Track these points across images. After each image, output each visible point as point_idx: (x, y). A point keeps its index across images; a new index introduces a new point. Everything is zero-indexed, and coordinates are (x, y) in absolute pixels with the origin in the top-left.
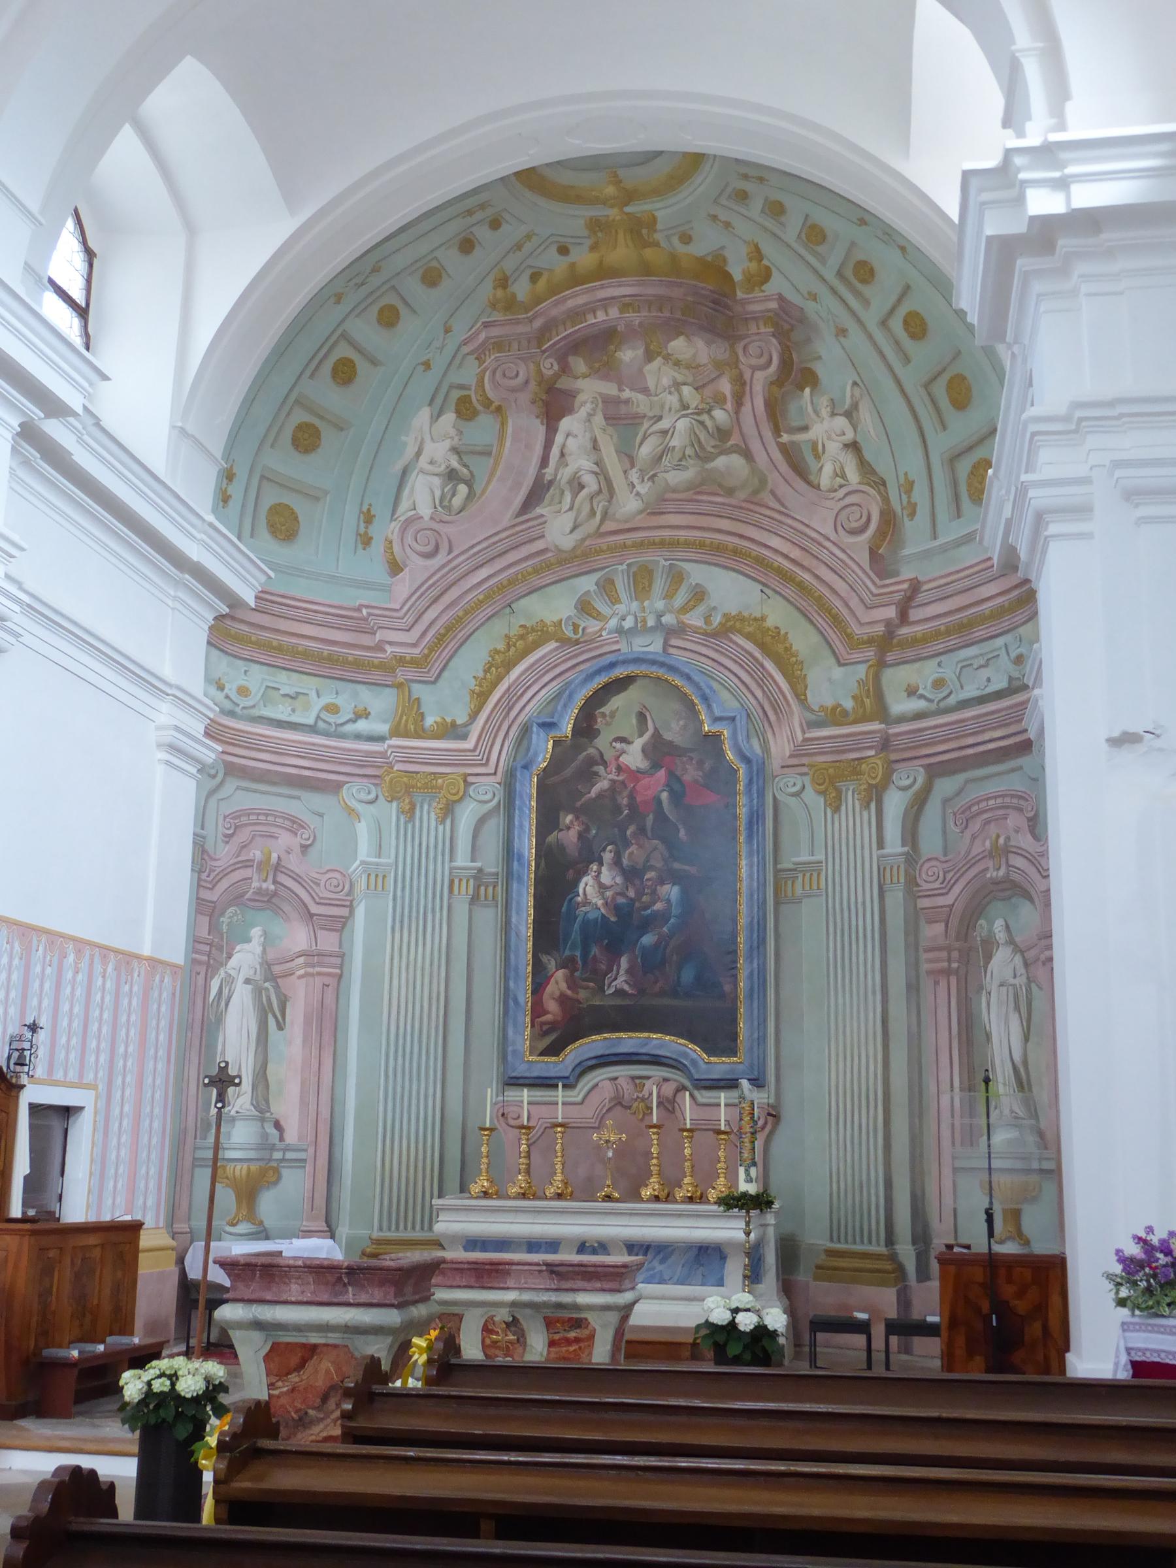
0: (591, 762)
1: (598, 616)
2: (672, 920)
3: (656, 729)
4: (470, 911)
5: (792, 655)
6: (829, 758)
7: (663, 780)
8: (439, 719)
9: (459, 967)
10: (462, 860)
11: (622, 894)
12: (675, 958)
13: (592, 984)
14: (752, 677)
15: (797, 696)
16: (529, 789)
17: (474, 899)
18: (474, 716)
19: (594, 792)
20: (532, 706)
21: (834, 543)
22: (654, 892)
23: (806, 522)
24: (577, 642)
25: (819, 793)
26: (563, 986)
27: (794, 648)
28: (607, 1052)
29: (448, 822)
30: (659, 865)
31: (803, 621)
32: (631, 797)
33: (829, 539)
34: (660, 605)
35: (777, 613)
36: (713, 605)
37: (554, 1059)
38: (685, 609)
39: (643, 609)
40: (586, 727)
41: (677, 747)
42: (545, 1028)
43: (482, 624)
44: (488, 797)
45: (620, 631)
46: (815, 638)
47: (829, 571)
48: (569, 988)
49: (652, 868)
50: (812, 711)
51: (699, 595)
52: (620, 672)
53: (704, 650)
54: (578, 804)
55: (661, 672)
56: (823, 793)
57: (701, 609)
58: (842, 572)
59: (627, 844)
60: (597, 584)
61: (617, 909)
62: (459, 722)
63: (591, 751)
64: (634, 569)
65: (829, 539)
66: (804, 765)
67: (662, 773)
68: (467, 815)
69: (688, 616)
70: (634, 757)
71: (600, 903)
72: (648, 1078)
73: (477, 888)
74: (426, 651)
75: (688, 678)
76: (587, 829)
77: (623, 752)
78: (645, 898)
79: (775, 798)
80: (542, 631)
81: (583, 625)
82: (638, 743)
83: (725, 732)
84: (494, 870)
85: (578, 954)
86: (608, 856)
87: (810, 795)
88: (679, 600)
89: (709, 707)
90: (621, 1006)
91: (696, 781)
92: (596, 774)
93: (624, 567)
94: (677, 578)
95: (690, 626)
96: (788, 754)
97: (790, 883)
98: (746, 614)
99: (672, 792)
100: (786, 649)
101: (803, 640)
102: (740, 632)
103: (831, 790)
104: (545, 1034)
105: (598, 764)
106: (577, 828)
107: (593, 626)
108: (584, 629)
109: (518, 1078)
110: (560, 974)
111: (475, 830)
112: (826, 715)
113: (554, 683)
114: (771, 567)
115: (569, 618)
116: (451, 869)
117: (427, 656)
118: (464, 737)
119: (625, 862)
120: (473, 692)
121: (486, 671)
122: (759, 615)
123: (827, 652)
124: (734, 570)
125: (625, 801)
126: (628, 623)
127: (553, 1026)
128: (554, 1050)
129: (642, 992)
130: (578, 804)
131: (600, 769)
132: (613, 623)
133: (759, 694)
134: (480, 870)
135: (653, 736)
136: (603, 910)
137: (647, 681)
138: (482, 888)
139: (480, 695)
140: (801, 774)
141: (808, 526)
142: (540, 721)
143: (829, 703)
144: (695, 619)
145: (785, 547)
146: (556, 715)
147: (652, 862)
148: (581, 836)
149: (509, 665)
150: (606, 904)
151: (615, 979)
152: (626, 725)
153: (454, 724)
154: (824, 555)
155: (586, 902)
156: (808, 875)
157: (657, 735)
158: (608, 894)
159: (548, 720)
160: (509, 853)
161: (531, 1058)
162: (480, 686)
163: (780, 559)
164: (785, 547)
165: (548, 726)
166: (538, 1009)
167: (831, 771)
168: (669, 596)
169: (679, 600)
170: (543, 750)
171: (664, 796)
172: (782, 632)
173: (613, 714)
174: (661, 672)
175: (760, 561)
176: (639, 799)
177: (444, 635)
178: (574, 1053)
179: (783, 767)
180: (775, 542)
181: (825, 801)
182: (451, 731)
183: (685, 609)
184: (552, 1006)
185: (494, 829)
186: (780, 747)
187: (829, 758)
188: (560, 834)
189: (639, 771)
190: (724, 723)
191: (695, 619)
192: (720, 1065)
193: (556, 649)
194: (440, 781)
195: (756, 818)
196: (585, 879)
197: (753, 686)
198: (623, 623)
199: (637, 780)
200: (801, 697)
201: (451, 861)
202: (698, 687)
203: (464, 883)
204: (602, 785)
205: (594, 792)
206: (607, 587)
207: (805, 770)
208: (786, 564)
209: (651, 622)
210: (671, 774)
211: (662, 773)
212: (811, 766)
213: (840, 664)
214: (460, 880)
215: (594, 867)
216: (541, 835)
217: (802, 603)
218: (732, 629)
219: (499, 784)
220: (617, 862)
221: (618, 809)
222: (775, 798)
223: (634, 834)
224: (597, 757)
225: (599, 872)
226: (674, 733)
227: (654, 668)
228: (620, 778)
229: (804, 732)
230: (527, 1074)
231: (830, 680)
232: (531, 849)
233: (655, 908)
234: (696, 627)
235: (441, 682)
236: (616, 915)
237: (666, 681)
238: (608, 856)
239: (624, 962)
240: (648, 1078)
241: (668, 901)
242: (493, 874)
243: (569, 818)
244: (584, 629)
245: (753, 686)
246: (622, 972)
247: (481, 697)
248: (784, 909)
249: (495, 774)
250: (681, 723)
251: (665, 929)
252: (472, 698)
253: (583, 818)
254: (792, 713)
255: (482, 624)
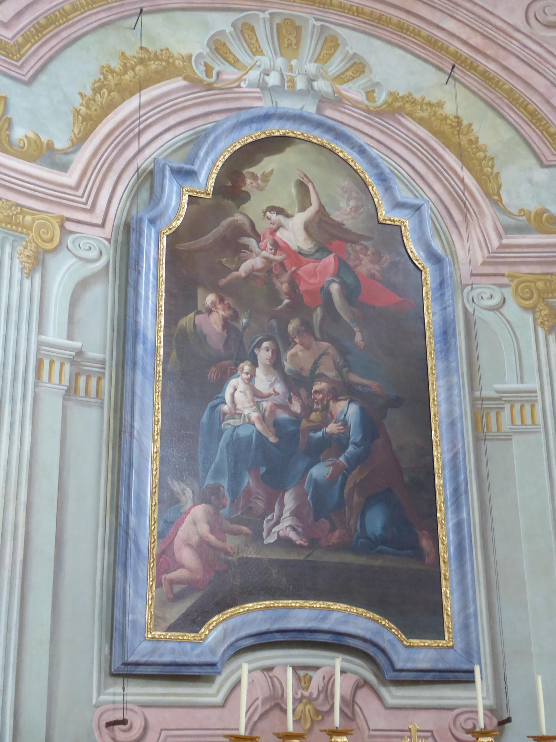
0: (238, 231)
1: (235, 63)
2: (351, 449)
3: (321, 207)
4: (64, 408)
5: (479, 149)
6: (538, 270)
7: (332, 268)
8: (31, 135)
9: (48, 487)
10: (55, 333)
11: (285, 408)
12: (356, 499)
13: (245, 529)
14: (428, 167)
15: (488, 195)
16: (153, 253)
17: (71, 392)
18: (78, 142)
19: (244, 268)
20: (160, 145)
21: (527, 35)
22: (326, 409)
23: (490, 9)
24: (210, 87)
25: (526, 309)
26: (204, 529)
27: (481, 142)
28: (276, 627)
29: (37, 277)
30: (331, 374)
31: (491, 114)
32: (293, 283)
33: (518, 31)
34: (311, 68)
35: (456, 101)
36: (377, 80)
37: (190, 636)
38: (340, 78)
39: (291, 69)
40: (232, 184)
41: (347, 231)
42: (177, 589)
43: (94, 30)
44: (93, 254)
45: (262, 86)
46: (507, 134)
47: (521, 64)
48: (212, 532)
49: (322, 377)
50: (510, 214)
51: (357, 67)
52: (275, 129)
53: (366, 129)
54: (223, 282)
55: (326, 139)
56: (532, 309)
57: (362, 81)
58: (540, 67)
59: (289, 343)
60: (233, 25)
61: (277, 425)
62: (58, 146)
63: (238, 217)
64: (278, 20)
65: (518, 31)
66: (503, 275)
67: (331, 259)
68: (64, 273)
69: (345, 86)
70: (294, 233)
71: (254, 416)
72: (316, 668)
73: (75, 377)
74: (20, 39)
75: (362, 151)
76: (235, 317)
77: (280, 226)
78: (314, 416)
79: (466, 310)
80: (167, 61)
81: (217, 69)
82: (299, 219)
83: (407, 223)
84: (98, 355)
85: (225, 483)
86: (264, 355)
87: (512, 310)
88: (335, 66)
89: (388, 189)
90: (287, 561)
91: (373, 276)
92: (247, 247)
93: (266, 15)
94: (330, 44)
95: (349, 99)
96: (480, 260)
97: (493, 415)
98: (418, 96)
99: (343, 285)
100: (470, 142)
101: (491, 133)
102: (410, 115)
103: (541, 306)
104: (178, 597)
105: (249, 236)
106: (219, 314)
107: (230, 74)
108: (218, 74)
109: (137, 664)
110: (199, 512)
111: (73, 296)
112: (529, 220)
113: (181, 129)
114: (447, 50)
115: (200, 56)
116: (40, 344)
117: (20, 46)
118: (64, 168)
119: (287, 365)
120: (78, 112)
121: (97, 91)
122: (434, 101)
123: (524, 151)
124: (400, 47)
125: (284, 287)
126: (273, 80)
127: (191, 586)
128: (193, 621)
129: (314, 543)
130: (223, 282)
131: (252, 242)
132: (254, 75)
133: (438, 187)
134: (80, 353)
135: (317, 212)
136: (259, 426)
137: (307, 146)
138: (82, 380)
139: (87, 118)
140: (501, 286)
141: (491, 13)
142: (176, 165)
143: (533, 207)
144: (354, 91)
145: (464, 33)
146: (198, 163)
147: (322, 369)
148: (226, 324)
149: (126, 92)
150: (263, 418)
151: (278, 523)
152: (286, 196)
153: (50, 147)
154: (514, 47)
155: (235, 413)
156: (517, 407)
157: (321, 210)
158: (266, 405)
159: (188, 167)
160: (126, 331)
161: (157, 634)
162: (88, 107)
163: (458, 44)
164: (464, 33)
165: (185, 174)
166: (166, 560)
167: (540, 285)
168: (322, 59)
169: (335, 66)
170: (175, 204)
171: (335, 288)
172: (465, 123)
173: (266, 177)
174: (326, 139)
175: (432, 43)
176: (303, 287)
177: (45, 27)
178: (215, 632)
179: (473, 275)
180: (450, 24)
181: (535, 320)
182: (43, 153)
183: (340, 78)
184: (187, 556)
185: (100, 302)
186: (469, 251)
187: (538, 270)
188: (199, 318)
189: (300, 252)
190: (406, 212)
191: (354, 91)
192: (420, 653)
193: (185, 88)
194: (28, 218)
195: (446, 333)
196: (233, 382)
197: (430, 178)
198: (267, 78)
199: (299, 265)
200: (494, 198)
201: (40, 331)
202: (372, 163)
203: (57, 366)
204: (253, 262)
205: (244, 268)
206: (245, 31)
207: (505, 280)
208: (465, 50)
209: (300, 84)
210: (341, 263)
211: (331, 259)
212: (512, 277)
213: (543, 165)
214: (52, 362)
215: (246, 367)
216: (173, 315)
217: (491, 96)
218: (400, 111)
219: (109, 240)
220: (276, 364)
221: (274, 297)
222: (466, 310)
223: (298, 332)
224: (248, 227)
225: (253, 375)
226: (343, 212)
227: (317, 133)
228: (278, 257)
229: (500, 237)
230: (155, 659)
231: (530, 181)
232: (157, 332)
233: (328, 430)
234: (356, 101)
235: (37, 86)
236: (277, 435)
237: (332, 151)
238: (264, 355)
239: (289, 500)
240: (316, 668)
241: (345, 423)
242: (95, 361)
243: (210, 298)
244: (218, 74)
245: (430, 178)
246: (286, 514)
247: (89, 122)
248: (491, 447)
249: (103, 225)
250: (352, 203)
251: (342, 459)
252: (75, 119)
253: (229, 301)
254: (482, 213)
255: (94, 30)
